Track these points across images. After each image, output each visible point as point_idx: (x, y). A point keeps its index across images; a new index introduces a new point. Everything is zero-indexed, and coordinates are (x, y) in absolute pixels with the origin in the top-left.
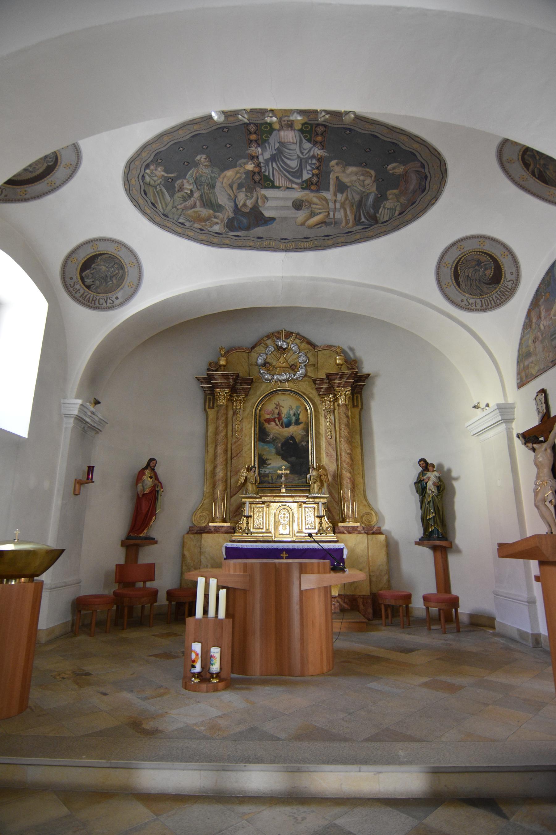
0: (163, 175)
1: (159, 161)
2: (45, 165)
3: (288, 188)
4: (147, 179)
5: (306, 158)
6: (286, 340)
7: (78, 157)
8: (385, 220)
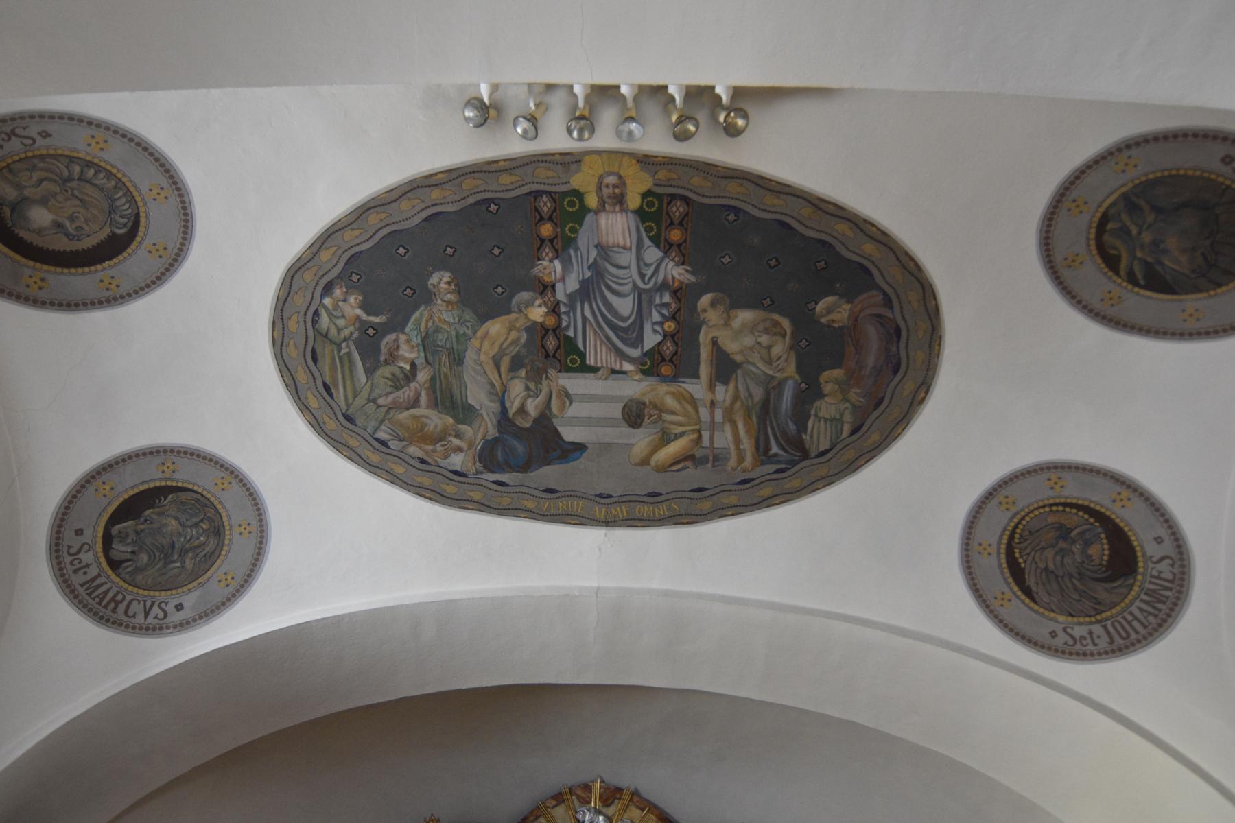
0: (358, 317)
1: (355, 278)
2: (107, 231)
3: (614, 372)
4: (324, 321)
5: (649, 290)
6: (604, 810)
7: (185, 233)
8: (822, 448)
